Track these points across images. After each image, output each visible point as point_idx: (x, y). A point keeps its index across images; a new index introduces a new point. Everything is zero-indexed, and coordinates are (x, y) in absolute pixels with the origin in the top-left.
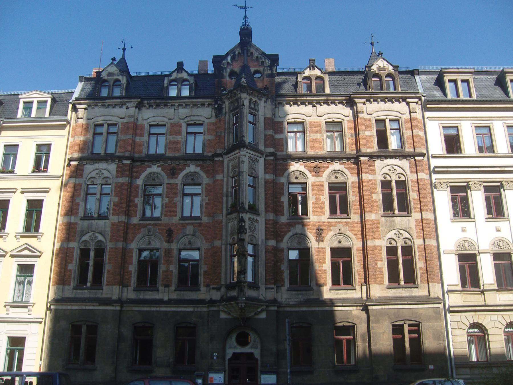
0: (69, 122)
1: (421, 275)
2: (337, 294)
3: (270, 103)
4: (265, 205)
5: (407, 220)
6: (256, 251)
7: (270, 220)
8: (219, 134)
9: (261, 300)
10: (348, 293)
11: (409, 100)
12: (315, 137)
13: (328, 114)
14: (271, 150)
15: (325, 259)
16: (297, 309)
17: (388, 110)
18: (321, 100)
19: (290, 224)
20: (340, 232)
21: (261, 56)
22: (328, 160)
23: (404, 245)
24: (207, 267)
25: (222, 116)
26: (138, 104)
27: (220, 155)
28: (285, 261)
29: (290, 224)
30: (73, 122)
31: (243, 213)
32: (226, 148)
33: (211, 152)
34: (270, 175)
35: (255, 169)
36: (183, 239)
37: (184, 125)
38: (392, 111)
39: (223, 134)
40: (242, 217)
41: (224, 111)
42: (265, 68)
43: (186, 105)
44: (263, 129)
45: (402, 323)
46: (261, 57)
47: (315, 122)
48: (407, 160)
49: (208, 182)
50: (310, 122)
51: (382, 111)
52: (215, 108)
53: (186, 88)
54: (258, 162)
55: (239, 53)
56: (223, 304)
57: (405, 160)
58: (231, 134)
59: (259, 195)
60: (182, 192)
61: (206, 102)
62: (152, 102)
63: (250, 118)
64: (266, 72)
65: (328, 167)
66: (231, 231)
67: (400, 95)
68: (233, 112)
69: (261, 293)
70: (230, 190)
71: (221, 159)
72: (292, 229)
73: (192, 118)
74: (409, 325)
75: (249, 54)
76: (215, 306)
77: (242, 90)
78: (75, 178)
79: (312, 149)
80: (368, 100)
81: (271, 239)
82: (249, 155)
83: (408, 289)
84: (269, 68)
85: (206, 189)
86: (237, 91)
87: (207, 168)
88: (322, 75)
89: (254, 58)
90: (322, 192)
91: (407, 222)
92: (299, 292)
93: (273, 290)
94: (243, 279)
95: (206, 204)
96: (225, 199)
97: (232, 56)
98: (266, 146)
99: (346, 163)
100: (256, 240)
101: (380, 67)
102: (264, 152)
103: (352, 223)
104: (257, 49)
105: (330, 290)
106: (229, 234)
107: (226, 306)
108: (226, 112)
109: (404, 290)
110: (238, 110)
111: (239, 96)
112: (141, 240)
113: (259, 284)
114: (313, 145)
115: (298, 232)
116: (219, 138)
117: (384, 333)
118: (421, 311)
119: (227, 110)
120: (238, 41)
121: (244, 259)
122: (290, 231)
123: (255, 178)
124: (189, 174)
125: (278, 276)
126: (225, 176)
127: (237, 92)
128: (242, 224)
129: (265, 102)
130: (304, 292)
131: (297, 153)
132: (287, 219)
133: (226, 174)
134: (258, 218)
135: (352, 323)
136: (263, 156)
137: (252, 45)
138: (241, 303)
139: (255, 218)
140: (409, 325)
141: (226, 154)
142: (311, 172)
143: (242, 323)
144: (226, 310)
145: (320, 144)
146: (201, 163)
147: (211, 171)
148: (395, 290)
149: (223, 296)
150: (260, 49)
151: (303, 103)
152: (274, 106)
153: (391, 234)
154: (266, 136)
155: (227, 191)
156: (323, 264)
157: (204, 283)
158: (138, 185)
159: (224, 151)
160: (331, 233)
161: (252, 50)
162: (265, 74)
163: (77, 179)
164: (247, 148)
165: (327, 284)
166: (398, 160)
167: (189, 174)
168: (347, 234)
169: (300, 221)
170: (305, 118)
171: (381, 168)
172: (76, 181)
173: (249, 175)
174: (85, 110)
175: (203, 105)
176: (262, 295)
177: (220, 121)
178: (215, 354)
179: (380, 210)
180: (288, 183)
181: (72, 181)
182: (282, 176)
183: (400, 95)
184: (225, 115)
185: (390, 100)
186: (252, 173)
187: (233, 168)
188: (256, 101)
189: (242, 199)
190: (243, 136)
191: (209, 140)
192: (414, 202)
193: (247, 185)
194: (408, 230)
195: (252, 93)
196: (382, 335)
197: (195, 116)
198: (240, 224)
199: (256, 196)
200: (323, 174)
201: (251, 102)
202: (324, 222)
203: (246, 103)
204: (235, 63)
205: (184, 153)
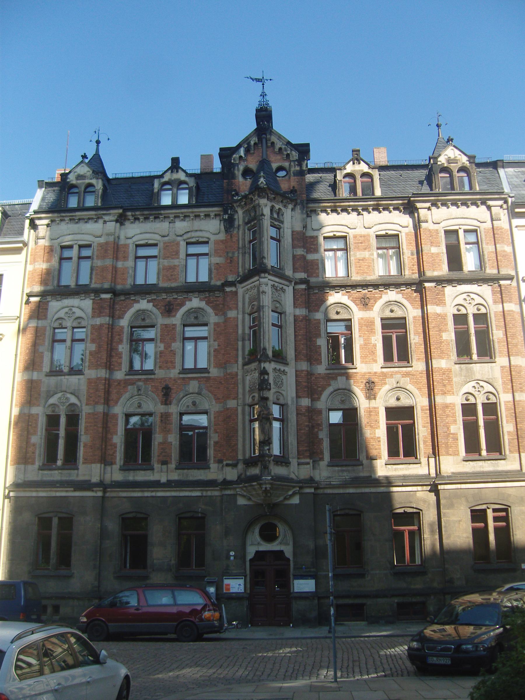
0: (26, 244)
1: (509, 442)
2: (396, 470)
3: (300, 211)
4: (296, 350)
5: (490, 367)
6: (285, 414)
7: (302, 371)
8: (230, 255)
9: (292, 479)
10: (410, 469)
11: (490, 203)
12: (362, 256)
13: (380, 224)
14: (302, 275)
15: (378, 422)
16: (341, 491)
17: (461, 217)
18: (370, 205)
19: (330, 376)
20: (398, 385)
21: (286, 147)
22: (380, 287)
23: (487, 402)
24: (219, 436)
25: (233, 230)
26: (118, 217)
27: (232, 284)
28: (324, 426)
29: (330, 376)
30: (31, 244)
31: (265, 362)
32: (241, 274)
33: (220, 280)
34: (301, 309)
35: (281, 302)
36: (184, 399)
37: (183, 244)
38: (467, 218)
39: (236, 255)
40: (264, 368)
41: (236, 223)
42: (292, 164)
43: (185, 216)
44: (291, 247)
45: (484, 507)
46: (285, 148)
47: (361, 237)
48: (489, 285)
49: (217, 321)
50: (355, 237)
51: (453, 219)
52: (225, 220)
53: (184, 194)
54: (284, 292)
55: (255, 144)
56: (241, 486)
57: (486, 285)
58: (247, 255)
59: (286, 337)
60: (182, 336)
61: (212, 211)
62: (137, 213)
63: (273, 232)
64: (293, 169)
65: (381, 297)
66: (250, 387)
67: (478, 197)
68: (249, 225)
69: (292, 470)
70: (247, 331)
71: (233, 289)
72: (332, 382)
73: (193, 234)
74: (494, 510)
75: (270, 145)
76: (230, 489)
77: (261, 194)
78: (36, 320)
79: (357, 273)
80: (434, 204)
81: (304, 397)
82: (273, 283)
83: (492, 461)
84: (296, 163)
85: (215, 330)
86: (254, 196)
87: (215, 302)
88: (370, 171)
89: (277, 150)
90: (372, 331)
91: (490, 370)
92: (344, 468)
93: (308, 466)
94: (267, 452)
95: (215, 350)
96: (240, 343)
97: (245, 148)
98: (295, 270)
99: (405, 291)
100: (284, 399)
101: (450, 157)
102: (293, 279)
103: (414, 373)
104: (280, 137)
105: (386, 464)
106: (247, 391)
107: (245, 489)
108: (239, 226)
109: (486, 463)
110: (255, 222)
111: (257, 202)
112: (128, 402)
113: (289, 458)
114: (360, 267)
115: (341, 386)
116: (231, 261)
117: (460, 521)
118: (510, 491)
119: (241, 222)
120: (255, 127)
121: (268, 424)
122: (330, 385)
123: (280, 314)
124: (191, 311)
125: (315, 447)
126: (241, 312)
127: (254, 197)
128: (264, 378)
129: (292, 210)
130: (350, 468)
131: (338, 278)
132: (326, 369)
133: (241, 310)
134: (286, 369)
135: (416, 508)
136: (291, 284)
137: (273, 132)
138: (266, 484)
139: (282, 368)
140: (494, 510)
141: (241, 282)
142: (357, 305)
143: (266, 511)
144: (245, 494)
145: (369, 266)
146: (207, 295)
147: (221, 306)
148: (475, 462)
149: (241, 474)
150: (284, 137)
151: (345, 210)
152: (305, 216)
153: (468, 387)
154: (294, 256)
155: (244, 333)
156: (376, 430)
157: (214, 457)
158: (122, 327)
159: (238, 278)
160: (387, 387)
161: (274, 139)
162: (292, 172)
163: (40, 322)
164: (269, 274)
165: (382, 457)
166: (476, 285)
167: (191, 311)
168: (407, 388)
169: (343, 371)
170: (348, 230)
171: (453, 298)
172: (38, 324)
173: (272, 311)
174: (47, 227)
175: (207, 216)
176: (294, 473)
177: (231, 237)
178: (232, 553)
179: (453, 355)
180: (325, 320)
181: (33, 324)
182: (317, 311)
183: (478, 197)
184: (238, 229)
185: (465, 203)
186: (277, 308)
187: (251, 302)
188: (280, 209)
189: (264, 344)
190: (264, 257)
191: (217, 264)
192: (498, 342)
193: (271, 324)
194: (490, 381)
195: (274, 198)
196: (457, 525)
197: (196, 231)
198: (262, 378)
199: (283, 339)
200: (373, 306)
201: (274, 211)
202: (376, 373)
203: (267, 211)
204: (250, 158)
205: (184, 282)
